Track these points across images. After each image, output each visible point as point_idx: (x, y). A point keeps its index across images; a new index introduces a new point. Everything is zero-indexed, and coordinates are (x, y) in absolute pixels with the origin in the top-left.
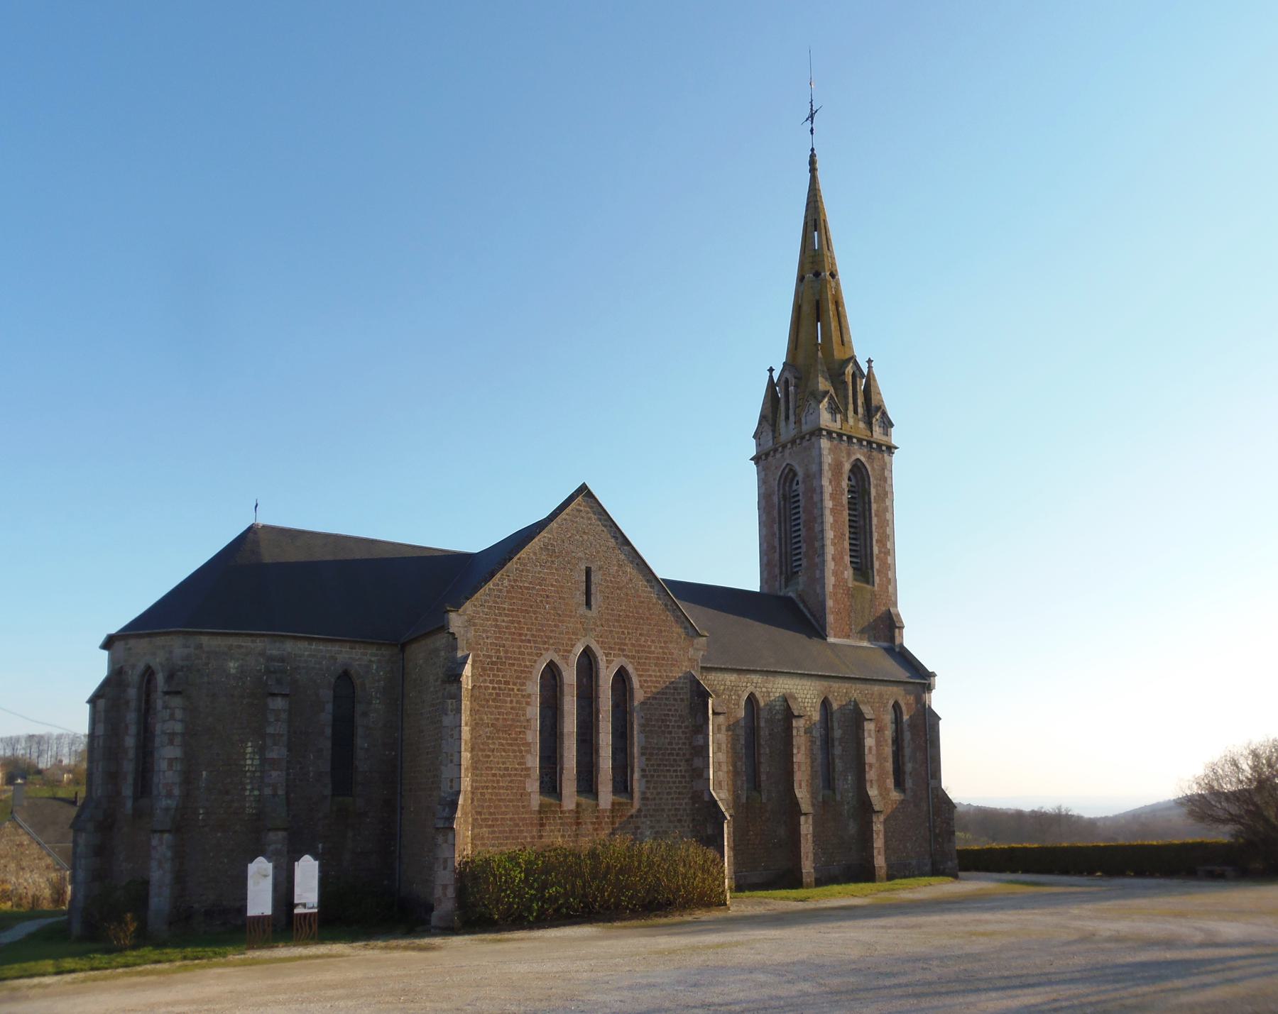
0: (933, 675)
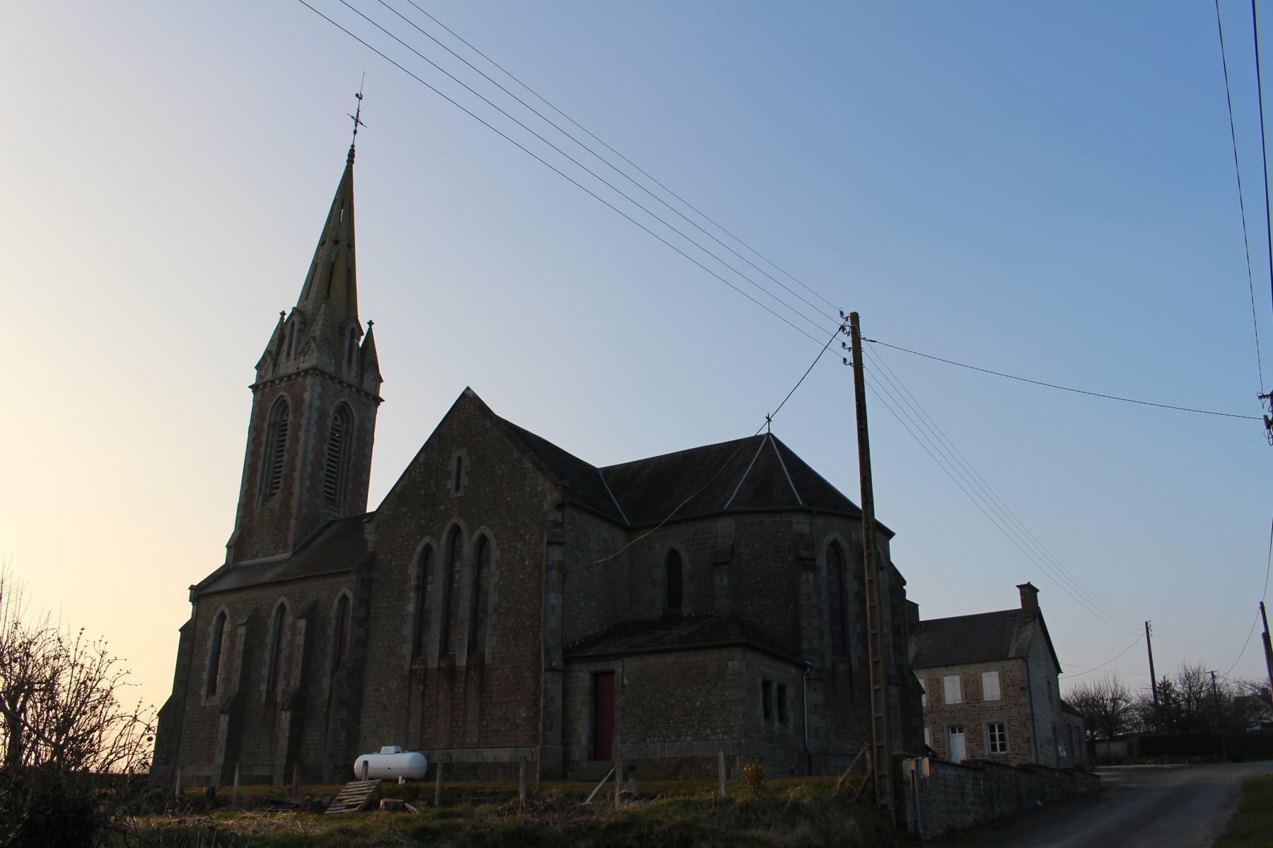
0: (192, 588)
